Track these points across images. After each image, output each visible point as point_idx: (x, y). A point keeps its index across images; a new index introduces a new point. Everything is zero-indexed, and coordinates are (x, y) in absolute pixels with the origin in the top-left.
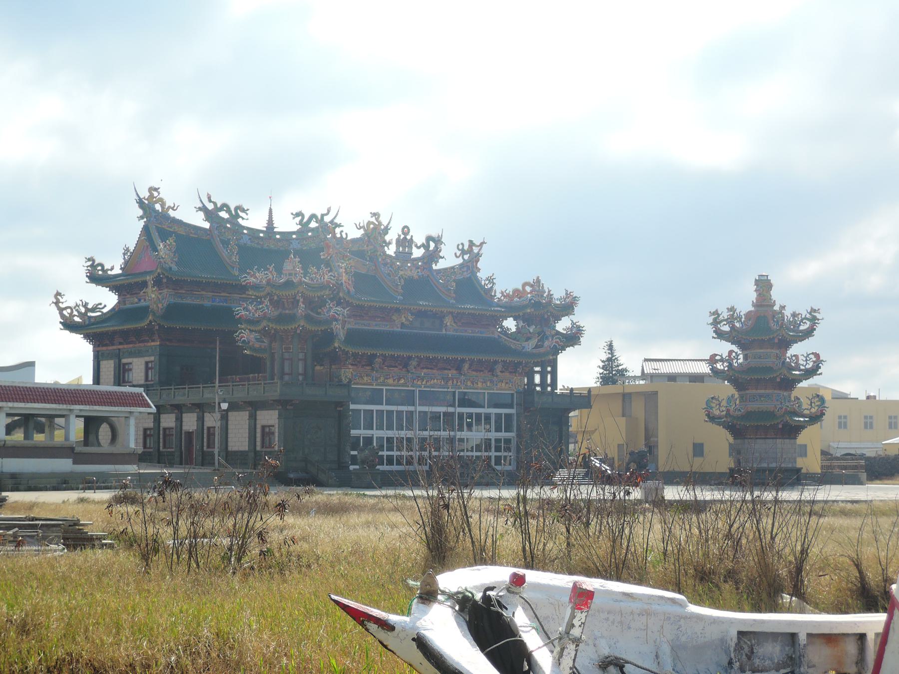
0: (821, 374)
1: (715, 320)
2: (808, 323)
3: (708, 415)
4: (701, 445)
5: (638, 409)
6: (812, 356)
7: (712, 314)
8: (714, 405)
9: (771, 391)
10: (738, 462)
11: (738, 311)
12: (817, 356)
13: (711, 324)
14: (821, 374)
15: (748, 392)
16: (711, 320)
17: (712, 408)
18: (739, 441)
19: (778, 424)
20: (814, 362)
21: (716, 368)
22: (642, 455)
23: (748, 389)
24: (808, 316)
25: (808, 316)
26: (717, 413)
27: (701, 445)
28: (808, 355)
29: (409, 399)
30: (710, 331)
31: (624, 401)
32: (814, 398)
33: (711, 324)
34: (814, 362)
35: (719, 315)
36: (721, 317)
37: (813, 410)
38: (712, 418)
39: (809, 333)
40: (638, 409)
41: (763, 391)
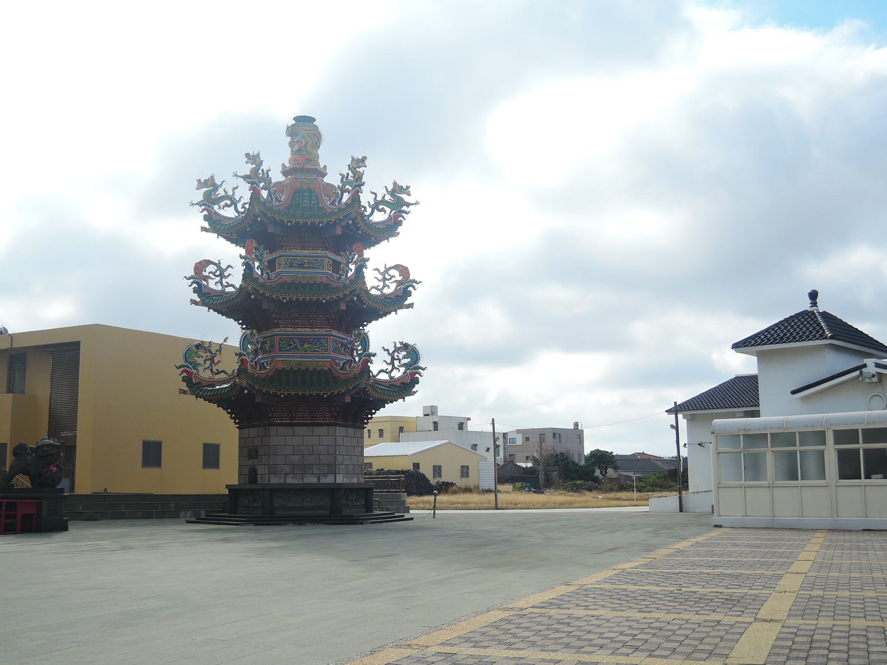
0: (411, 306)
1: (207, 195)
2: (388, 210)
3: (188, 380)
4: (217, 447)
5: (40, 383)
6: (394, 272)
7: (201, 184)
8: (200, 361)
9: (323, 331)
10: (252, 475)
11: (265, 167)
12: (404, 270)
13: (200, 204)
14: (411, 306)
15: (276, 331)
16: (199, 196)
17: (196, 365)
18: (253, 431)
19: (344, 394)
20: (399, 283)
21: (207, 287)
22: (44, 454)
23: (277, 326)
24: (388, 197)
25: (388, 197)
26: (205, 375)
27: (217, 447)
28: (387, 270)
29: (773, 555)
30: (198, 219)
31: (11, 368)
32: (397, 350)
33: (200, 204)
34: (399, 283)
35: (216, 187)
36: (221, 192)
37: (397, 374)
38: (195, 386)
39: (390, 229)
40: (40, 383)
41: (307, 331)
